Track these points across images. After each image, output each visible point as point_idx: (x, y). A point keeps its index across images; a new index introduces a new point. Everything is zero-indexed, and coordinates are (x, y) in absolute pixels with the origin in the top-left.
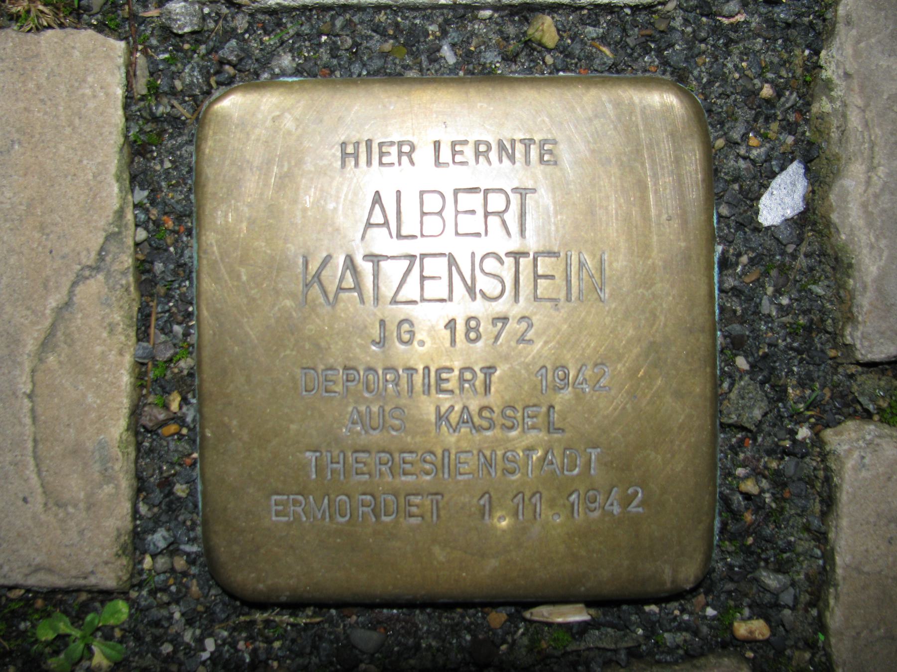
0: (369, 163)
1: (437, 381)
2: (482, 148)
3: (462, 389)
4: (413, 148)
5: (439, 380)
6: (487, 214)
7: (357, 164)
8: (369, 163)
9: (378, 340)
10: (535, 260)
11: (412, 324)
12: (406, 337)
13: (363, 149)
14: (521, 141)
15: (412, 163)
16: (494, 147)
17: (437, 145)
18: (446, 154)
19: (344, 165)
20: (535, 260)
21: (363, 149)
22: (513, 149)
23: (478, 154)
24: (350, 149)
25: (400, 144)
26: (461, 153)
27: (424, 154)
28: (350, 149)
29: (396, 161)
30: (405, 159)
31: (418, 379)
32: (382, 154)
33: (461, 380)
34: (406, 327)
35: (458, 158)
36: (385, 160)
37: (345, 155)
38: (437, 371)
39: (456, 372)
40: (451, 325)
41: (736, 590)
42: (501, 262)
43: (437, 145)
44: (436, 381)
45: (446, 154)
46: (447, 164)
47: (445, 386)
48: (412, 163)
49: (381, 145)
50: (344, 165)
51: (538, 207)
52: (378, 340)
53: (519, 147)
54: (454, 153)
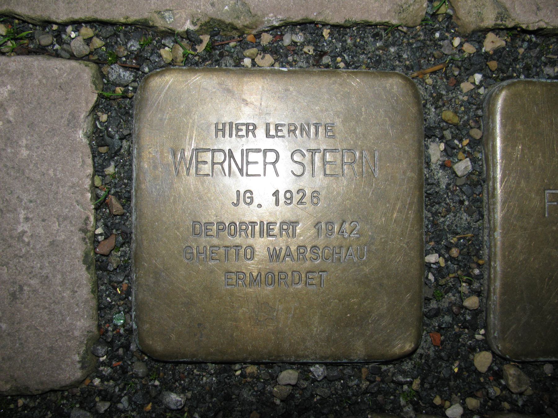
0: (231, 135)
1: (266, 229)
2: (293, 128)
3: (281, 235)
4: (255, 127)
5: (268, 229)
6: (213, 164)
7: (224, 136)
8: (231, 135)
9: (235, 202)
10: (324, 155)
11: (251, 192)
12: (248, 201)
13: (227, 127)
14: (313, 124)
15: (254, 136)
16: (299, 127)
17: (268, 125)
18: (273, 132)
19: (217, 136)
20: (324, 155)
21: (227, 127)
22: (309, 129)
23: (289, 131)
24: (220, 127)
25: (247, 125)
26: (281, 130)
27: (261, 132)
28: (220, 127)
29: (287, 135)
30: (250, 134)
31: (257, 228)
32: (238, 130)
33: (281, 229)
34: (248, 195)
35: (280, 134)
36: (240, 133)
37: (217, 130)
38: (268, 224)
39: (278, 225)
40: (276, 194)
41: (228, 376)
42: (304, 155)
43: (268, 125)
44: (267, 230)
45: (273, 132)
46: (273, 137)
47: (271, 233)
48: (254, 136)
49: (277, 126)
50: (217, 136)
51: (283, 363)
52: (235, 202)
53: (313, 129)
54: (277, 130)
